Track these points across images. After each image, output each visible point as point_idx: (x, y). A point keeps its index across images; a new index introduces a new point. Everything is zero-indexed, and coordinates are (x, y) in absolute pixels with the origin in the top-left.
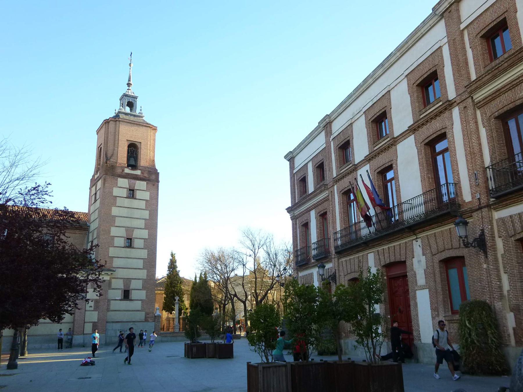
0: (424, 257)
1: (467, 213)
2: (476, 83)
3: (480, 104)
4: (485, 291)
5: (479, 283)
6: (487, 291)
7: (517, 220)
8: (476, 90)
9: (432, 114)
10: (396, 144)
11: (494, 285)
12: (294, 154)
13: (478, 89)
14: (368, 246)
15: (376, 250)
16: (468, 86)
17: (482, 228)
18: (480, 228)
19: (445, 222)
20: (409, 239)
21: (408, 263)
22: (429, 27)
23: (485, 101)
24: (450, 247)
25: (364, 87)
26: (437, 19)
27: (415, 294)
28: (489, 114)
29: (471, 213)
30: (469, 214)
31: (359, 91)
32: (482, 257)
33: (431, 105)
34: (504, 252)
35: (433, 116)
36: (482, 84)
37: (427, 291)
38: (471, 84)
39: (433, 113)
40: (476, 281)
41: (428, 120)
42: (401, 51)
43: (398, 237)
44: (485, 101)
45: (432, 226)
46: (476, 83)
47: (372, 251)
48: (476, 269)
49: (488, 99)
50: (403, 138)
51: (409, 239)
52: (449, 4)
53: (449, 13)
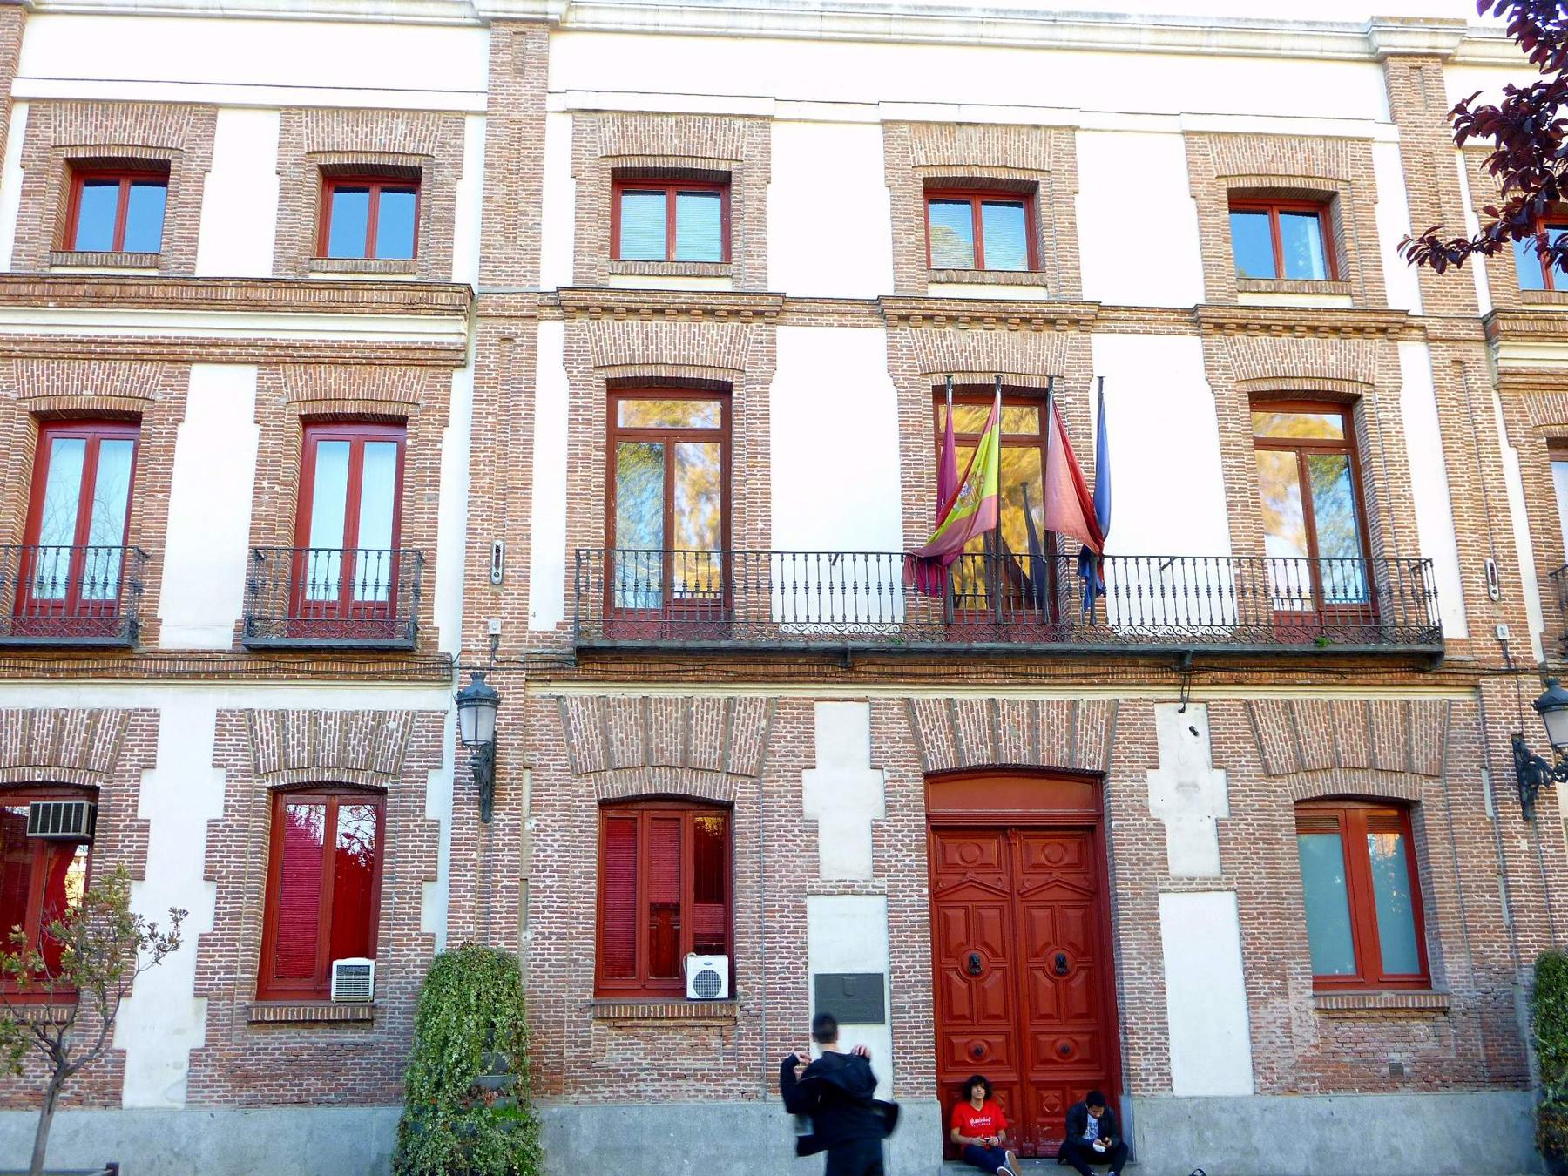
0: (1221, 774)
1: (1462, 671)
2: (1536, 319)
3: (1514, 380)
4: (1524, 922)
5: (1487, 895)
6: (1529, 921)
7: (331, 727)
8: (1523, 339)
9: (1327, 317)
10: (1092, 329)
11: (1560, 906)
12: (571, 17)
13: (1534, 339)
14: (851, 669)
15: (942, 696)
16: (1508, 315)
17: (1518, 731)
18: (1512, 729)
19: (1354, 677)
20: (1135, 695)
21: (1117, 785)
22: (1315, 50)
23: (1531, 380)
24: (638, 758)
25: (896, 27)
26: (1353, 52)
27: (1154, 906)
28: (1532, 420)
29: (1477, 677)
30: (1472, 678)
31: (791, 23)
32: (1515, 818)
33: (621, 265)
34: (225, 815)
35: (1327, 324)
36: (1553, 334)
37: (1225, 904)
38: (1520, 316)
39: (1333, 318)
40: (1473, 885)
41: (1294, 326)
42: (1167, 38)
43: (1085, 676)
44: (1531, 380)
45: (1294, 675)
46: (1536, 319)
47: (862, 694)
48: (1477, 848)
49: (1543, 380)
50: (1137, 326)
51: (1135, 695)
52: (1429, 48)
53: (1410, 68)
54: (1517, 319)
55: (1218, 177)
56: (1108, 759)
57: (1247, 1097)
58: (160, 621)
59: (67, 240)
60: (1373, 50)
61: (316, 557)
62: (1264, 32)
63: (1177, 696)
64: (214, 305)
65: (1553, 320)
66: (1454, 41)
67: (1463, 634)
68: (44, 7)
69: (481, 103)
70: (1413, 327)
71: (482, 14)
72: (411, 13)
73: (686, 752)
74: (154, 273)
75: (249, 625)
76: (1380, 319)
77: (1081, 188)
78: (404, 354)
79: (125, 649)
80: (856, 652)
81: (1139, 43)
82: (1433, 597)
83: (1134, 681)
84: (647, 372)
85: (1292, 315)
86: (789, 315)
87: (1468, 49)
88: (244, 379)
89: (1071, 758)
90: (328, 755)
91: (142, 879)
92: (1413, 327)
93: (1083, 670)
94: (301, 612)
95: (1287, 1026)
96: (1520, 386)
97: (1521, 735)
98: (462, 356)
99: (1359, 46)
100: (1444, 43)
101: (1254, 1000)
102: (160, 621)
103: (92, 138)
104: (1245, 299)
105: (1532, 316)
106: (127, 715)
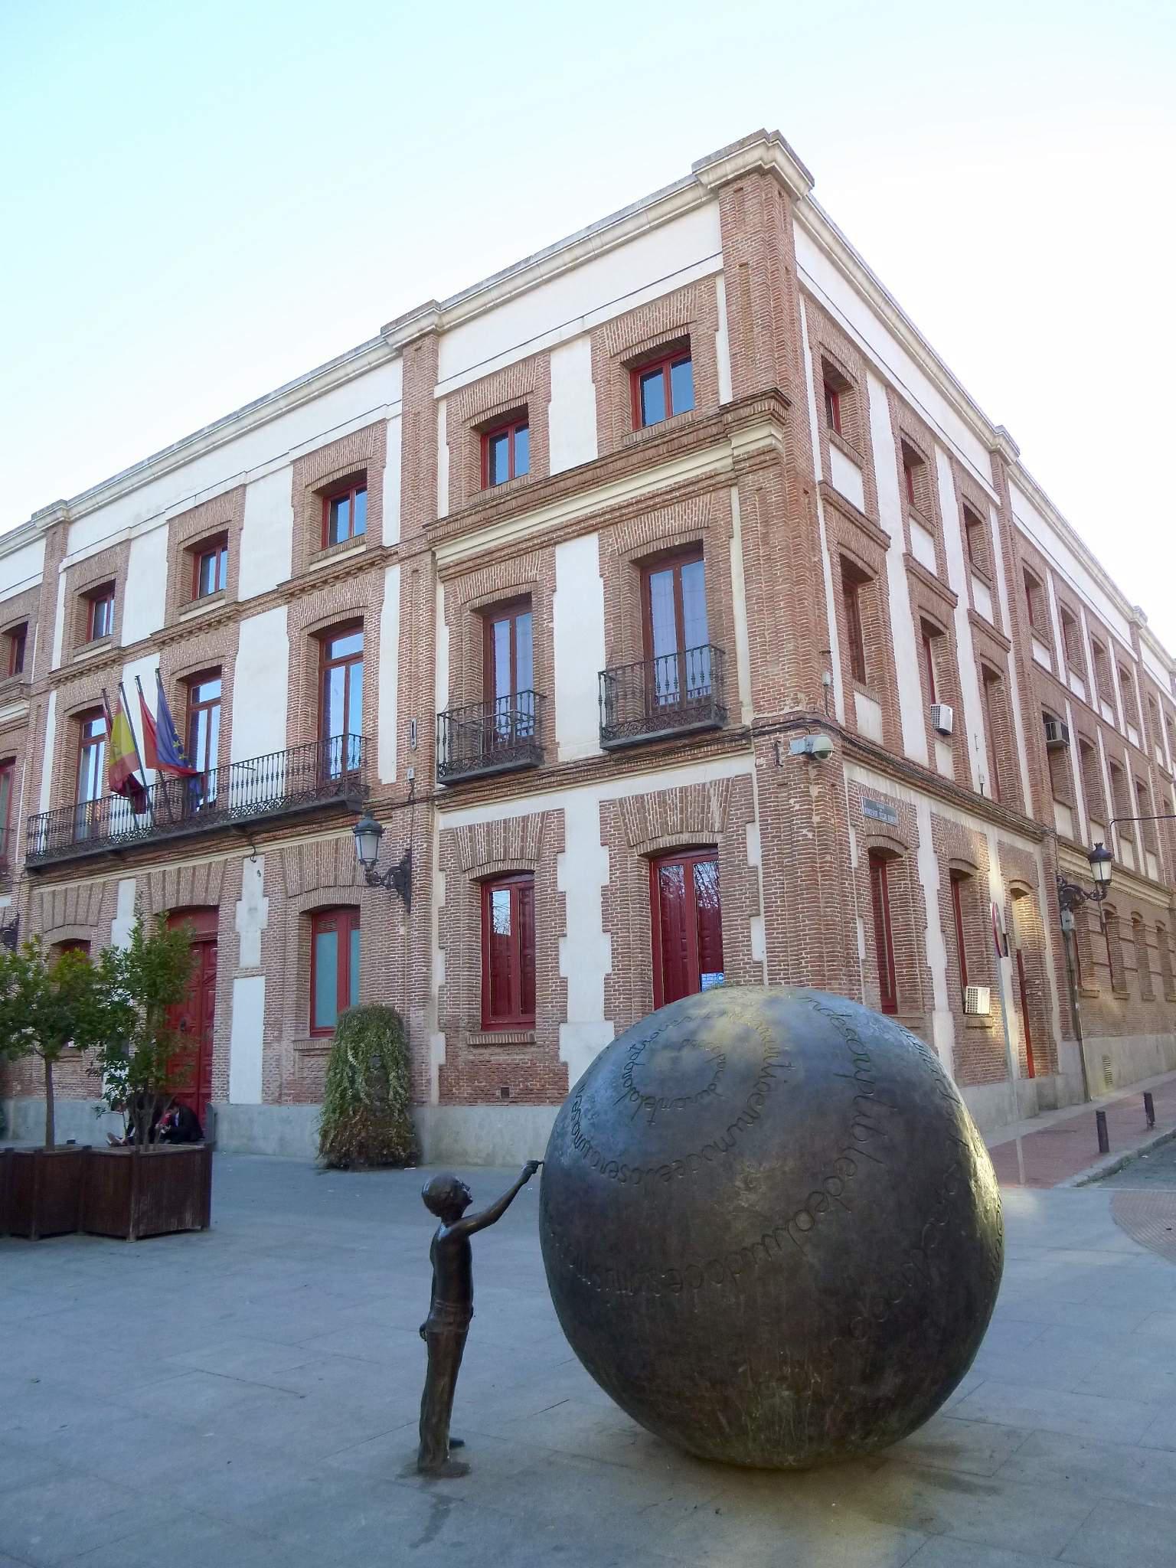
14: (124, 860)
18: (405, 847)
25: (179, 456)
31: (329, 379)
38: (438, 525)
42: (292, 398)
45: (298, 829)
54: (437, 528)
55: (306, 487)
56: (220, 898)
57: (259, 1105)
58: (558, 743)
59: (639, 419)
60: (439, 325)
61: (692, 656)
62: (335, 369)
63: (252, 852)
64: (566, 493)
65: (437, 528)
66: (434, 319)
67: (393, 779)
68: (446, 327)
69: (717, 264)
70: (391, 555)
71: (395, 347)
72: (675, 207)
73: (76, 918)
74: (222, 603)
75: (606, 733)
76: (367, 558)
77: (245, 527)
78: (683, 491)
79: (715, 728)
80: (126, 849)
81: (369, 364)
82: (260, 782)
83: (690, 758)
84: (199, 668)
85: (322, 573)
86: (128, 657)
87: (446, 319)
88: (590, 544)
89: (177, 902)
90: (498, 852)
91: (565, 936)
92: (391, 555)
93: (208, 844)
94: (653, 715)
95: (278, 1060)
96: (453, 576)
97: (410, 850)
98: (27, 720)
99: (386, 350)
100: (427, 324)
101: (267, 1044)
102: (558, 743)
103: (639, 338)
104: (183, 618)
105: (445, 522)
106: (545, 815)
